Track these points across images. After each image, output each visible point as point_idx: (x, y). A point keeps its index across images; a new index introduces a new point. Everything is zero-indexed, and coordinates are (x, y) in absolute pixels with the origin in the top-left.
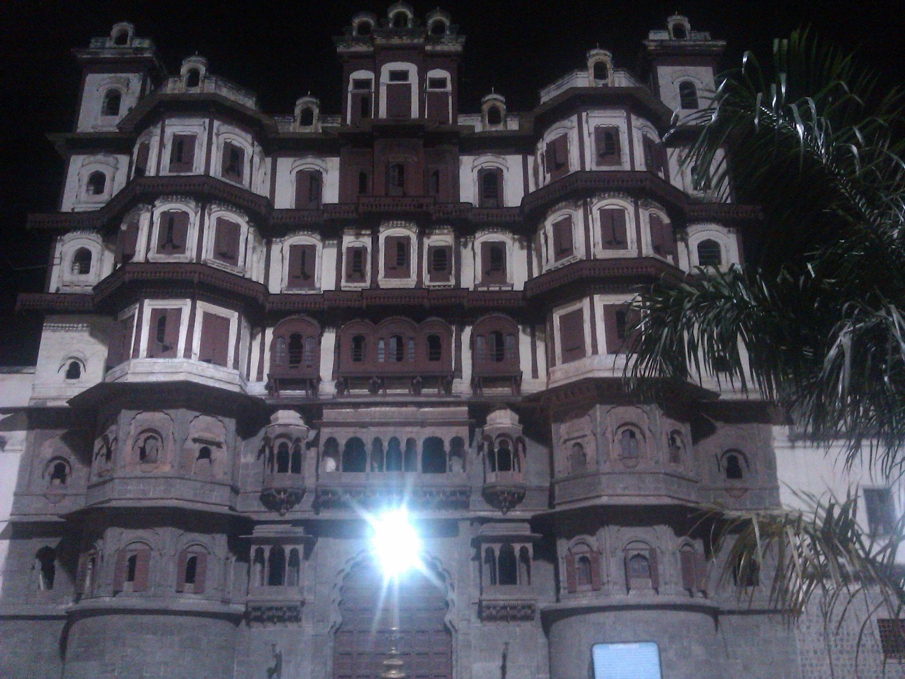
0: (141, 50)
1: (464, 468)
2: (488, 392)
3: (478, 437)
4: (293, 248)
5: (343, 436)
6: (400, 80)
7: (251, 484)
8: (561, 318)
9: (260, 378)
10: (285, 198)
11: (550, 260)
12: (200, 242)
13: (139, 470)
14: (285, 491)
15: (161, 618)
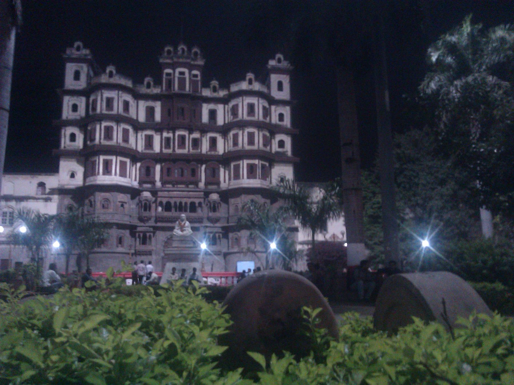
0: (86, 55)
1: (202, 211)
2: (210, 187)
3: (206, 202)
4: (146, 135)
5: (165, 201)
6: (183, 74)
7: (135, 215)
8: (234, 166)
9: (135, 180)
10: (142, 118)
11: (231, 147)
12: (117, 138)
13: (103, 211)
14: (147, 217)
15: (111, 254)
